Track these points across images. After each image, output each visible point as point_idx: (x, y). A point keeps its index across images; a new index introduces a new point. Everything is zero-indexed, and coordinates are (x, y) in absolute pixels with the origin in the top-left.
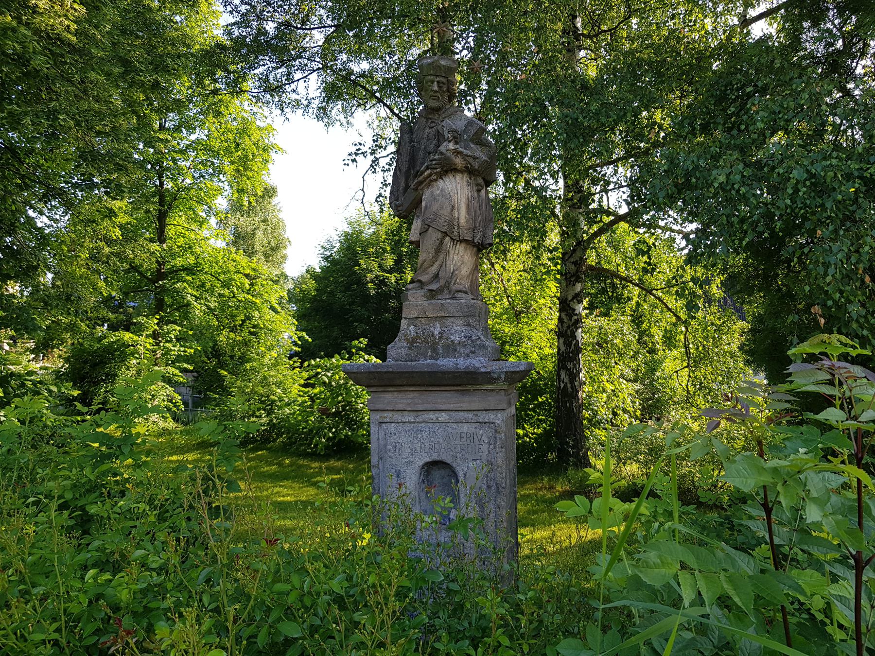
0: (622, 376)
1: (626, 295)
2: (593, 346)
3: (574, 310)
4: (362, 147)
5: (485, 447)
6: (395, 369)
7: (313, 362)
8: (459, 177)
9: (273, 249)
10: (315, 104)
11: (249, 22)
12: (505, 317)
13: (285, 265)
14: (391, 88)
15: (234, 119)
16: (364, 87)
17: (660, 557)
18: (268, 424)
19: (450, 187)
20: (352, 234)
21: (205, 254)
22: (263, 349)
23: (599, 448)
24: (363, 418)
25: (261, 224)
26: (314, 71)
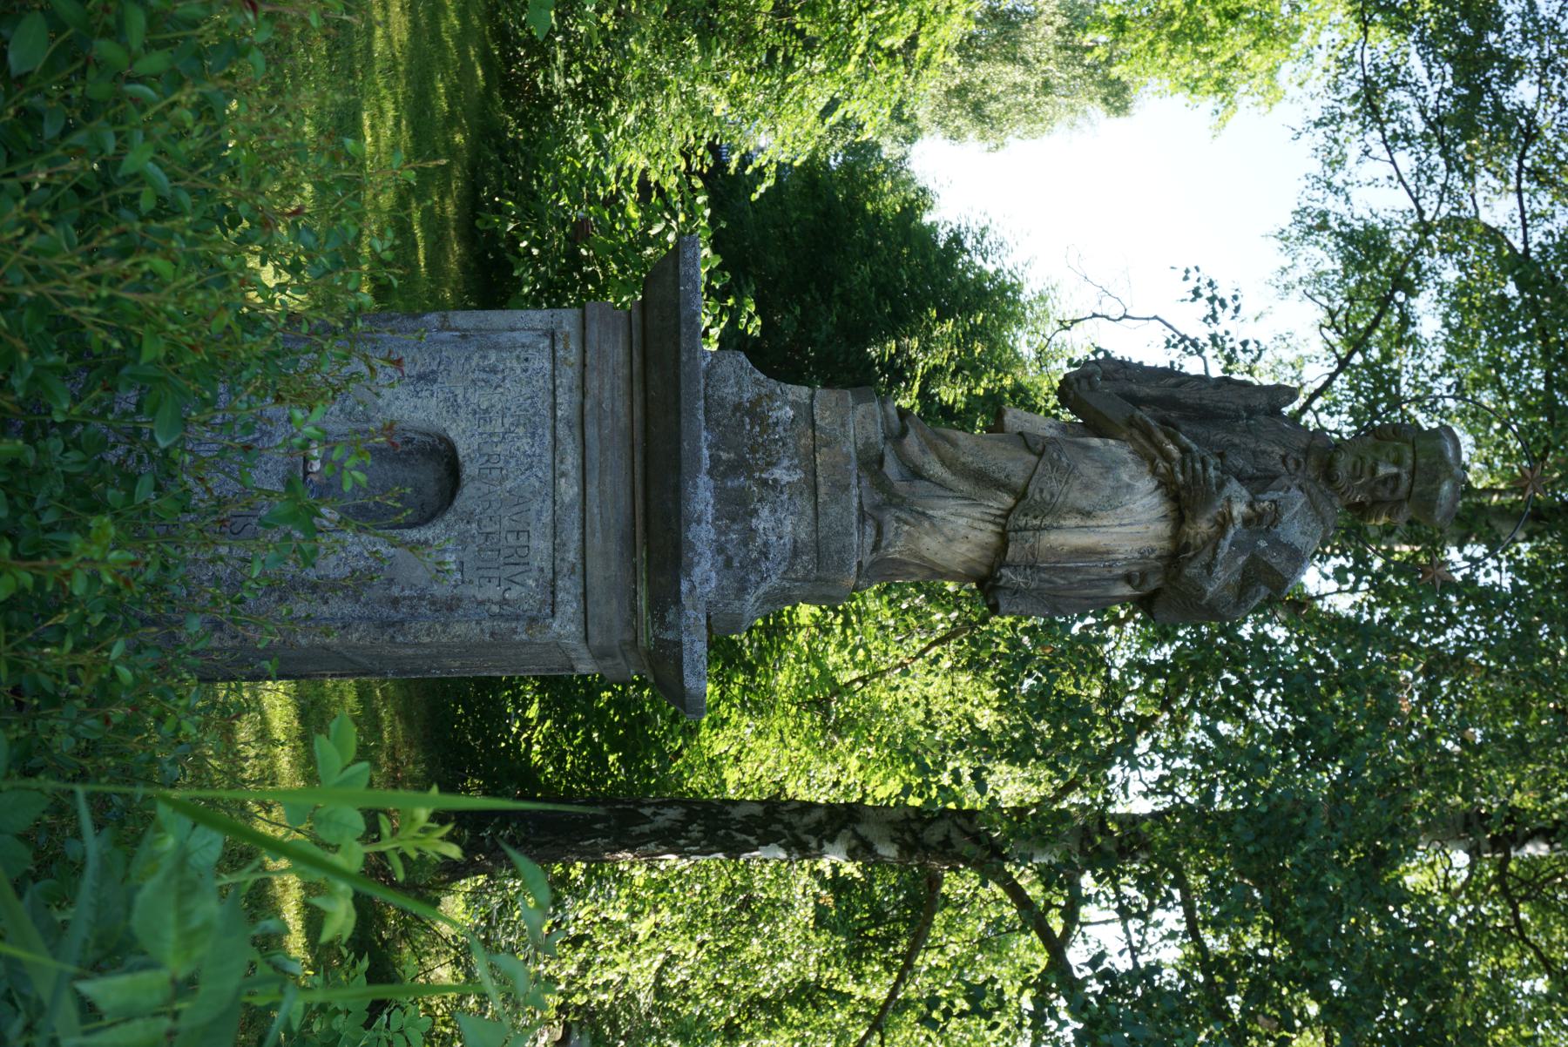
0: (670, 961)
1: (868, 969)
2: (743, 889)
3: (832, 840)
5: (493, 592)
6: (685, 369)
8: (1163, 529)
9: (977, 107)
10: (1334, 204)
11: (1539, 41)
12: (815, 672)
16: (1375, 323)
17: (207, 926)
18: (549, 93)
20: (1015, 302)
22: (734, 79)
23: (495, 902)
25: (1039, 79)
26: (1416, 201)
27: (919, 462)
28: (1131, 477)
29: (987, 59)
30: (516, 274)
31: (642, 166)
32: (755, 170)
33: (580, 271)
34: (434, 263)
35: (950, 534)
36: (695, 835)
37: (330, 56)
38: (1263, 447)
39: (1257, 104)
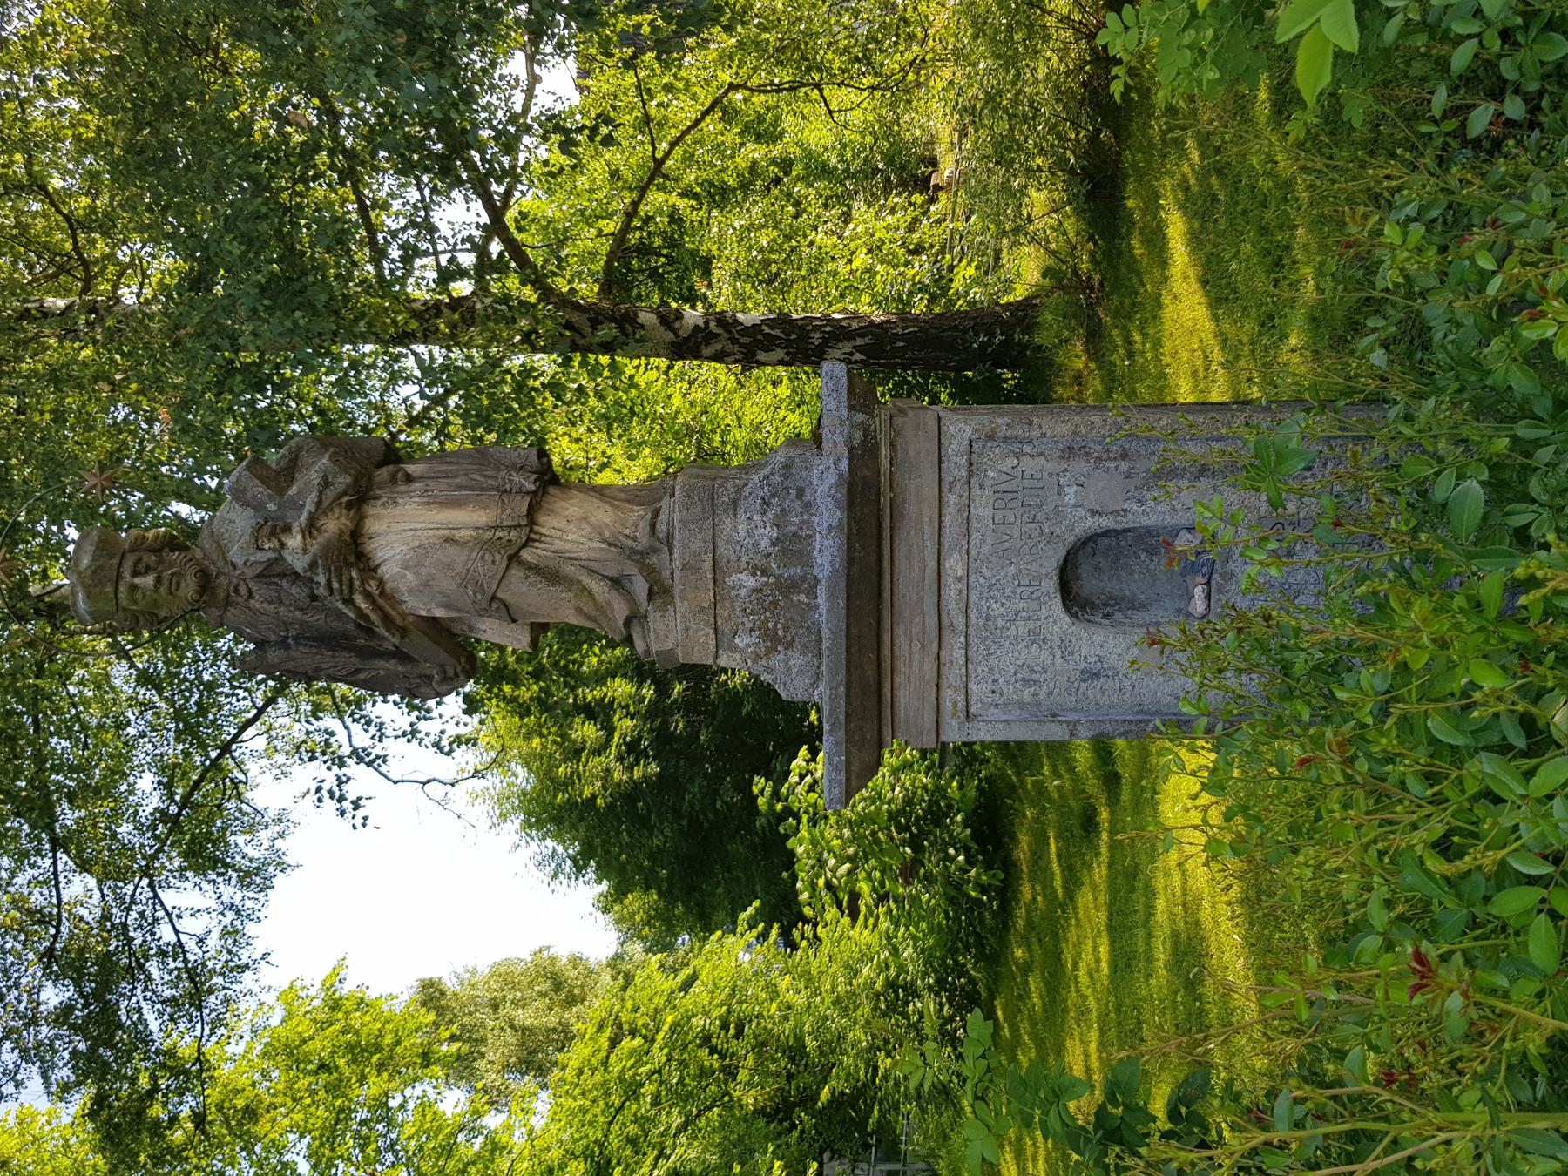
3: (697, 327)
4: (326, 786)
5: (1029, 465)
6: (841, 678)
7: (804, 896)
8: (371, 526)
9: (557, 987)
10: (231, 892)
11: (39, 1044)
13: (592, 960)
14: (199, 724)
15: (265, 1074)
16: (196, 785)
18: (937, 994)
19: (398, 547)
20: (528, 813)
21: (565, 1136)
24: (925, 787)
25: (501, 1013)
26: (156, 896)
27: (613, 592)
28: (404, 576)
29: (549, 1030)
30: (968, 831)
31: (857, 929)
32: (755, 926)
33: (911, 833)
34: (1041, 840)
35: (584, 525)
36: (817, 335)
37: (1139, 1023)
38: (271, 608)
39: (303, 988)
